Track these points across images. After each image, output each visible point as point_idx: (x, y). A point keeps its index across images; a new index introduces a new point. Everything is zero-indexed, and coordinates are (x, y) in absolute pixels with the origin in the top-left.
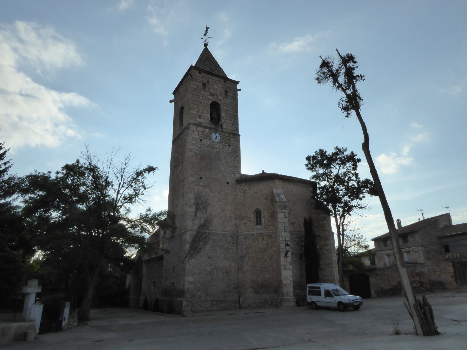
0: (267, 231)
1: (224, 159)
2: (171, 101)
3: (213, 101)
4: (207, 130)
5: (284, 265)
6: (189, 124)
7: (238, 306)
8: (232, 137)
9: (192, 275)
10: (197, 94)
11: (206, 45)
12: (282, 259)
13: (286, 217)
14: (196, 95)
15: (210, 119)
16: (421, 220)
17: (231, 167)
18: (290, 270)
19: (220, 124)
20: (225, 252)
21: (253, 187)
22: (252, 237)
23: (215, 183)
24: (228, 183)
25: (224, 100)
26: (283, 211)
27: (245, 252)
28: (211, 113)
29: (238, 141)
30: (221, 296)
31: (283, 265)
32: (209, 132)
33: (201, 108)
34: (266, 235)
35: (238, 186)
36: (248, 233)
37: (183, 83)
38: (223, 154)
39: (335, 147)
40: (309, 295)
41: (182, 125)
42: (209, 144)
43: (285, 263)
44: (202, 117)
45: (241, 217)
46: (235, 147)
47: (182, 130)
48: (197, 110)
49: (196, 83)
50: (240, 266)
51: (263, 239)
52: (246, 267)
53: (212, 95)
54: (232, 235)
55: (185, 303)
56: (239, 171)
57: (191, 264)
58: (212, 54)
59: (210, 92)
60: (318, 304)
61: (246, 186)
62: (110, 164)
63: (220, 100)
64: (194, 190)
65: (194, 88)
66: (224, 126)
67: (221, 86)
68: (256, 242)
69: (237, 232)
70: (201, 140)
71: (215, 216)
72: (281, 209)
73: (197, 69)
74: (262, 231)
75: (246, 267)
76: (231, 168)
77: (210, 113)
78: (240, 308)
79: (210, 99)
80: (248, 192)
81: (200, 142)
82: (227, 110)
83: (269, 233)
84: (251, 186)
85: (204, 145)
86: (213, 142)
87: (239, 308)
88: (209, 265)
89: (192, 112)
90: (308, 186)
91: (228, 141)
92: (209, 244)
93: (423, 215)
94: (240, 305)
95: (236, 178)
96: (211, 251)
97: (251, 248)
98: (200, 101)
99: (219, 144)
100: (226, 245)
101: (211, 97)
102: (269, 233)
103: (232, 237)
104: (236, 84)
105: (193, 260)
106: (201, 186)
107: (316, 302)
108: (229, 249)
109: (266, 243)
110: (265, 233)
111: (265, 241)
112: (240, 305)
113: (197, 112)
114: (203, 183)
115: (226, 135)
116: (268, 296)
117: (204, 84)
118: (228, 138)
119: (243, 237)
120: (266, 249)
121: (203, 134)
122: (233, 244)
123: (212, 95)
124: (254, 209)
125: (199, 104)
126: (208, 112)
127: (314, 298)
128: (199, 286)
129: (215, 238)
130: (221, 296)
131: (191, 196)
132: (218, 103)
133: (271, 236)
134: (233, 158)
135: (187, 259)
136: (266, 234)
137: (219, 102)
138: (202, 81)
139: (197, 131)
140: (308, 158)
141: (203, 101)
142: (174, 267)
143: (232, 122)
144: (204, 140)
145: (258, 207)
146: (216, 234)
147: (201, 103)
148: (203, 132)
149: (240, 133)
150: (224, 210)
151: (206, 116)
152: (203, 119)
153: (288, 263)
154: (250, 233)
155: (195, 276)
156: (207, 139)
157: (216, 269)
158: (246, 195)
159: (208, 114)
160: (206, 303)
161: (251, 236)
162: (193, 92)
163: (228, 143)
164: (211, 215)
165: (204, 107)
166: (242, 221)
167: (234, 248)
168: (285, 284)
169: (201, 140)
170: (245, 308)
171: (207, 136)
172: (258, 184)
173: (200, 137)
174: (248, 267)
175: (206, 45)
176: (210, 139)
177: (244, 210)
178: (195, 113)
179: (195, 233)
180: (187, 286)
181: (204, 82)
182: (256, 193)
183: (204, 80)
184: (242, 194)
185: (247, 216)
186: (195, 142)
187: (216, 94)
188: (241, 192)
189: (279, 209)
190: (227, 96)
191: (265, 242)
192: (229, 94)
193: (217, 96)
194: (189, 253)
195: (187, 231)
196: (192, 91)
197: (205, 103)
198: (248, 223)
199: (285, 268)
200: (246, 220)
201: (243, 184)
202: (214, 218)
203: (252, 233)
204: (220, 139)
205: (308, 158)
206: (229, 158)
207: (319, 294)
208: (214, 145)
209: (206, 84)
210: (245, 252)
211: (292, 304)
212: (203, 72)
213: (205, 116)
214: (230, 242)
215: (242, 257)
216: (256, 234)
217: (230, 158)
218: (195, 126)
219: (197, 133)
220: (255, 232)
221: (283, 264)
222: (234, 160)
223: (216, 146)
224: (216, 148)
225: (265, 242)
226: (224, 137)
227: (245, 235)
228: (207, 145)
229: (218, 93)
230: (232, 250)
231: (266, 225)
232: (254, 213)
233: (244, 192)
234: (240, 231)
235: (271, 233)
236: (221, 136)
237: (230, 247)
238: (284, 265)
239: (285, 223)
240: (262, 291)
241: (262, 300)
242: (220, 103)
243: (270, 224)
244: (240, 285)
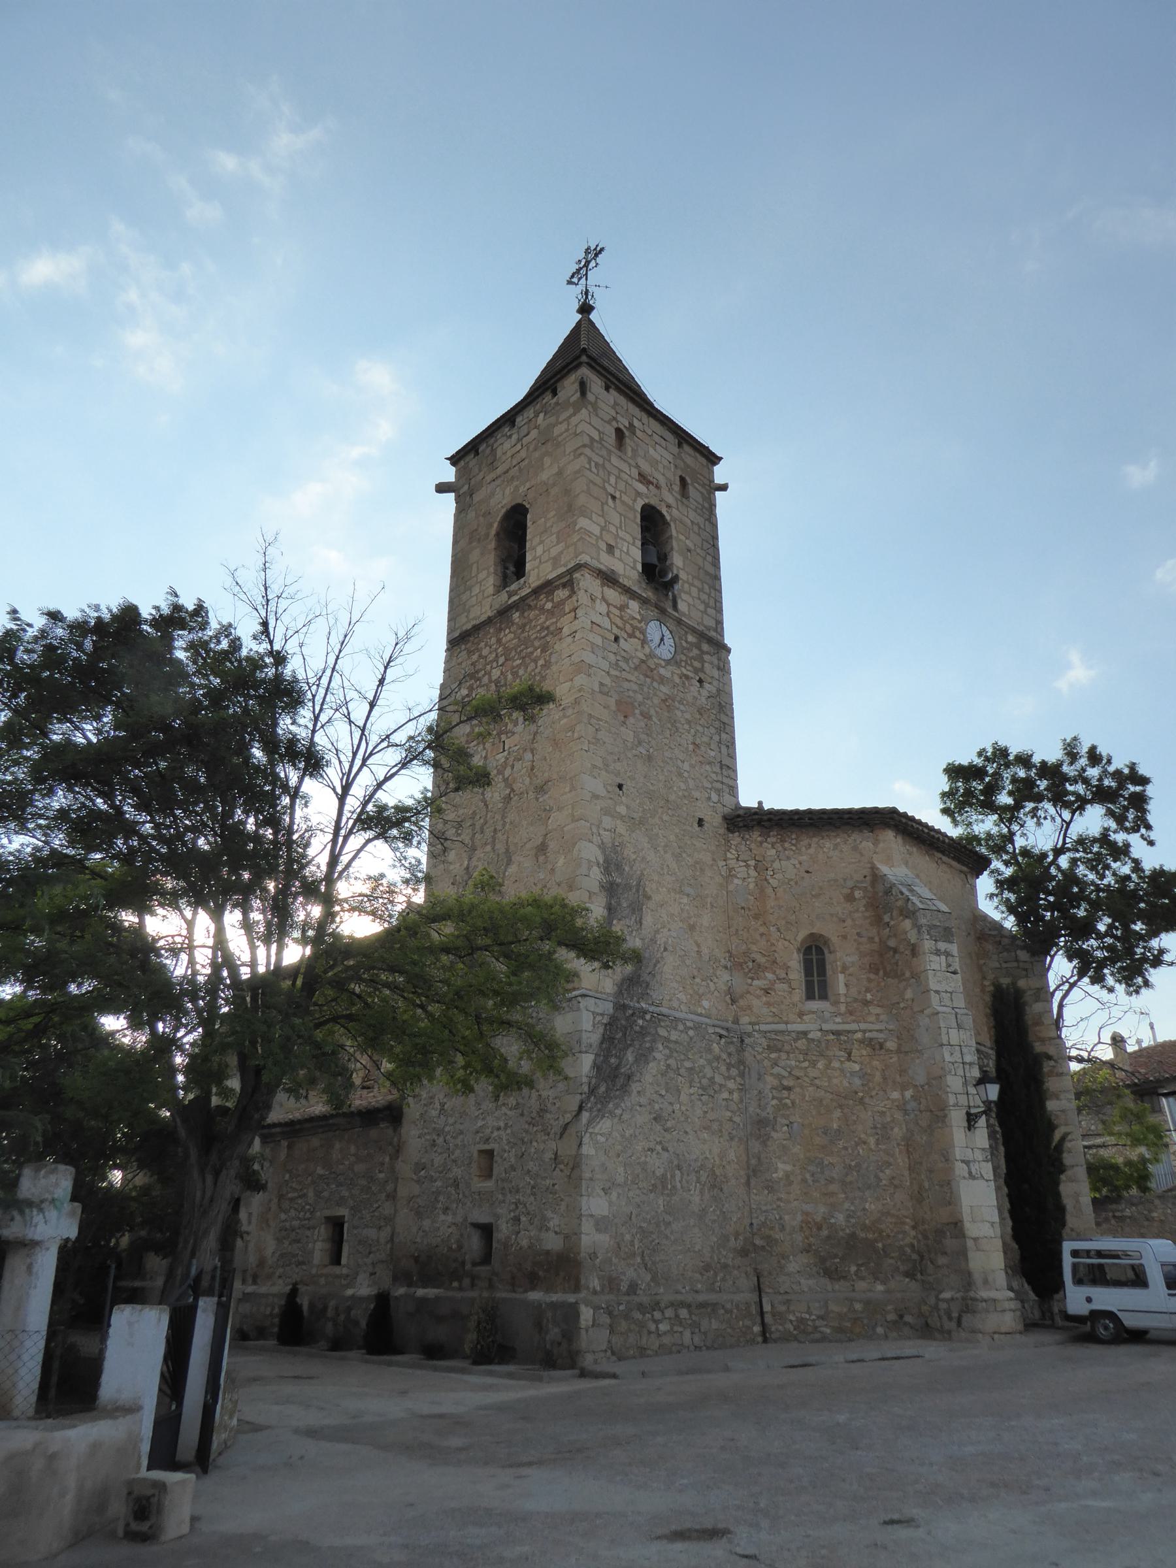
0: (863, 1026)
1: (686, 727)
2: (442, 488)
3: (647, 501)
4: (634, 606)
5: (967, 1163)
6: (579, 567)
7: (757, 1329)
8: (707, 653)
9: (603, 1189)
10: (600, 461)
11: (585, 309)
12: (959, 1134)
13: (955, 973)
14: (597, 464)
15: (640, 568)
16: (1144, 1045)
17: (710, 763)
18: (987, 1181)
19: (671, 597)
20: (703, 1098)
21: (794, 848)
22: (801, 1044)
23: (665, 818)
24: (701, 822)
25: (678, 509)
26: (942, 946)
27: (774, 1102)
28: (643, 544)
29: (724, 668)
30: (699, 1286)
31: (963, 1161)
32: (639, 612)
33: (615, 518)
34: (861, 1042)
35: (735, 839)
36: (782, 1027)
37: (519, 420)
38: (682, 707)
39: (1065, 740)
40: (1078, 1282)
41: (520, 571)
42: (643, 661)
43: (969, 1155)
44: (617, 553)
45: (750, 964)
46: (719, 690)
47: (516, 598)
48: (601, 521)
49: (595, 421)
50: (753, 1162)
51: (850, 1054)
52: (780, 1165)
53: (643, 478)
54: (724, 1032)
55: (586, 1315)
56: (731, 783)
57: (602, 1139)
58: (611, 345)
59: (637, 466)
60: (1130, 1321)
61: (766, 841)
62: (340, 651)
63: (669, 506)
64: (602, 832)
65: (592, 439)
66: (682, 606)
67: (670, 458)
68: (820, 1065)
69: (736, 1021)
70: (616, 639)
71: (665, 949)
72: (936, 941)
73: (598, 372)
74: (839, 1023)
75: (780, 1165)
76: (708, 767)
77: (639, 543)
78: (765, 1337)
79: (639, 494)
80: (776, 865)
81: (615, 645)
82: (689, 550)
83: (870, 1031)
84: (787, 845)
85: (626, 660)
86: (651, 655)
87: (760, 1339)
88: (659, 1148)
89: (583, 522)
90: (965, 869)
91: (697, 664)
92: (655, 1059)
93: (1152, 1028)
94: (763, 1324)
95: (727, 810)
96: (663, 1093)
97: (798, 1090)
98: (610, 490)
99: (669, 667)
100: (708, 1072)
101: (641, 488)
102: (870, 1031)
103: (723, 1040)
104: (710, 465)
105: (605, 1125)
106: (622, 817)
107: (1120, 1314)
108: (717, 1087)
109: (861, 1069)
110: (856, 1031)
111: (855, 1062)
112: (763, 1324)
113: (603, 529)
114: (628, 807)
115: (690, 638)
116: (880, 1287)
117: (619, 433)
118: (695, 652)
119: (765, 1043)
120: (861, 1094)
121: (621, 618)
122: (729, 1066)
123: (643, 478)
124: (802, 934)
125: (607, 503)
126: (634, 538)
127: (1107, 1298)
128: (628, 1237)
129: (674, 1036)
130: (699, 1286)
131: (590, 852)
132: (663, 516)
133: (881, 1046)
134: (713, 730)
135: (585, 1115)
136: (859, 1035)
137: (664, 511)
138: (614, 419)
139: (604, 599)
140: (955, 772)
141: (617, 495)
142: (490, 1154)
143: (704, 597)
144: (626, 640)
145: (819, 928)
146: (677, 1019)
147: (614, 498)
148: (622, 608)
149: (728, 640)
150: (692, 928)
151: (627, 553)
152: (620, 560)
153: (979, 1155)
154: (790, 1027)
155: (614, 1195)
156: (636, 637)
157: (679, 1167)
158: (768, 877)
159: (633, 544)
160: (657, 1315)
161: (795, 1040)
162: (587, 451)
163: (696, 671)
164: (653, 940)
165: (621, 515)
166: (753, 979)
167: (731, 1085)
168: (975, 1239)
169: (616, 639)
170: (786, 1338)
171: (634, 628)
172: (815, 840)
173: (614, 627)
174: (788, 1168)
175: (585, 309)
176: (644, 642)
177: (762, 935)
178: (596, 530)
179: (609, 1008)
180: (591, 1239)
181: (622, 427)
182: (807, 872)
183: (619, 418)
184: (753, 873)
185: (775, 962)
186: (598, 641)
187: (655, 481)
188: (747, 866)
189: (928, 937)
190: (687, 498)
191: (857, 1067)
192: (691, 490)
193: (658, 487)
194: (592, 1091)
195: (579, 999)
196: (584, 446)
197: (623, 503)
198: (779, 986)
199: (970, 1173)
200: (770, 976)
201: (756, 835)
202: (665, 954)
203: (801, 1027)
204: (673, 650)
205: (955, 772)
206: (700, 729)
207: (1138, 1279)
208: (658, 665)
209: (627, 433)
210: (774, 1102)
211: (1009, 1320)
212: (618, 389)
213: (625, 549)
214: (718, 1058)
215: (761, 1126)
216: (819, 1034)
217: (703, 726)
218: (598, 582)
219: (603, 608)
220: (809, 1025)
221: (963, 1158)
222: (716, 738)
223: (662, 671)
224: (662, 680)
225: (857, 1067)
226: (684, 644)
227: (774, 1037)
228: (635, 661)
229: (662, 481)
230: (725, 1095)
231: (856, 1000)
232: (799, 950)
233: (760, 866)
234: (745, 1020)
235: (880, 1031)
236: (676, 639)
237: (718, 1079)
238: (967, 1163)
239: (951, 993)
240: (853, 1269)
241: (858, 1306)
242: (668, 518)
243: (869, 996)
244: (758, 1242)
